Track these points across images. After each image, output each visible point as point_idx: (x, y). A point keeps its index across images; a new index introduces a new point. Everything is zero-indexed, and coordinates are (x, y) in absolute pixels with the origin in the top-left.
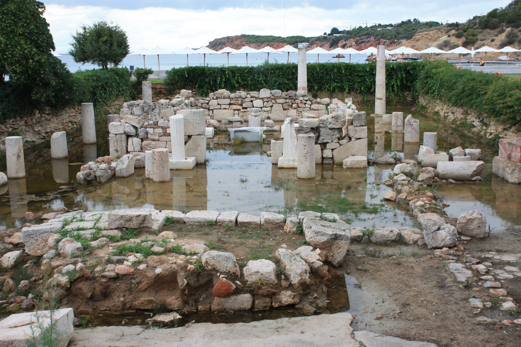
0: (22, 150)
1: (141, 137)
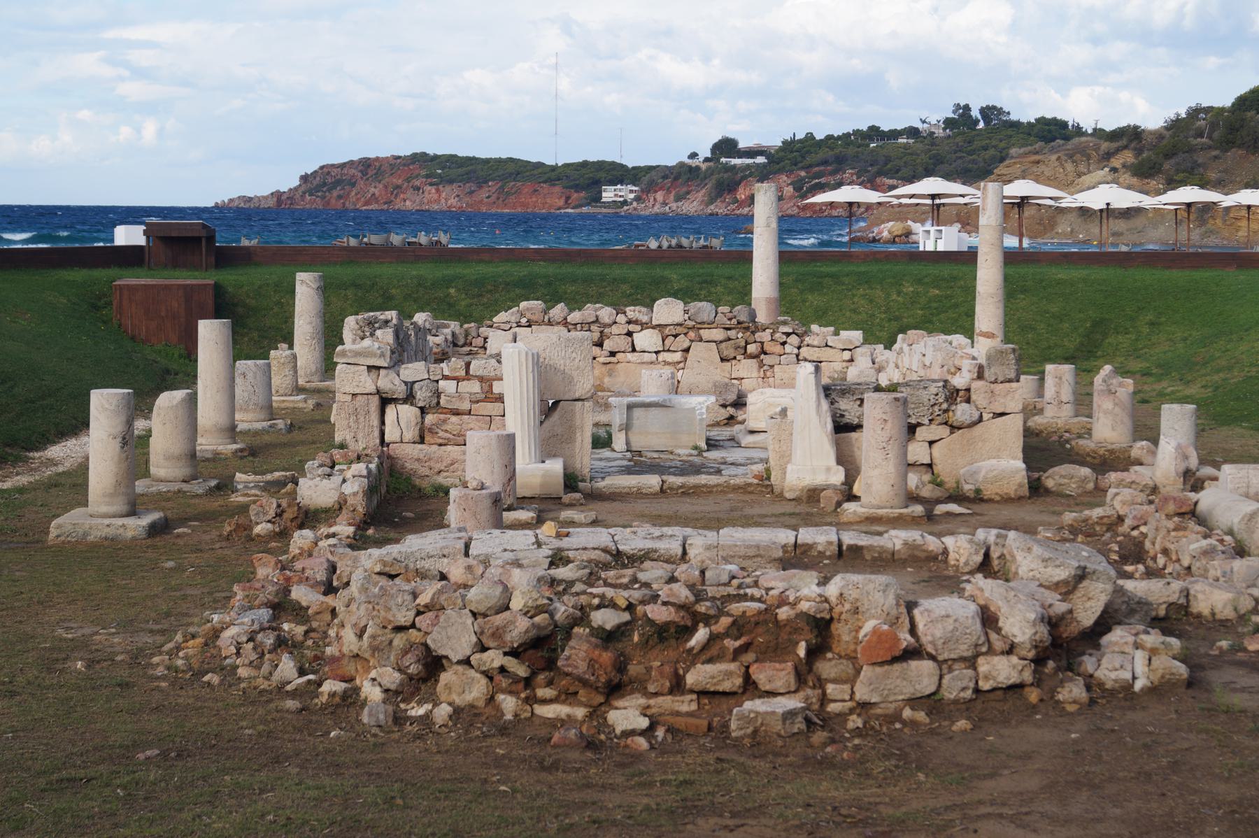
1: (421, 404)
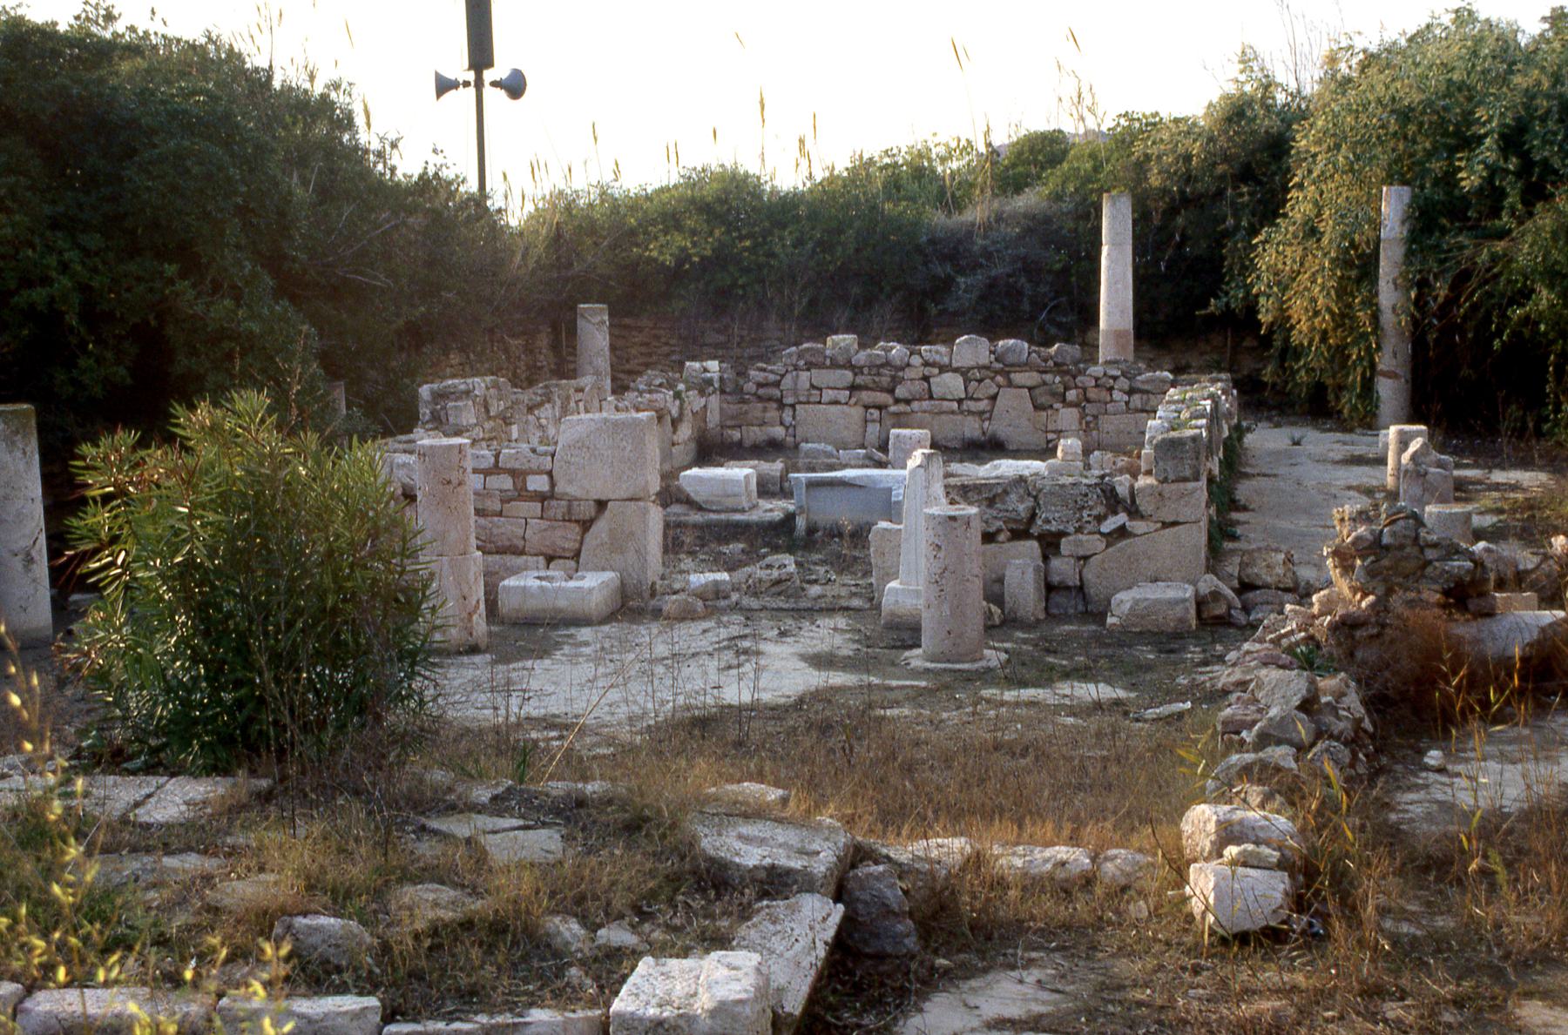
0: (43, 537)
